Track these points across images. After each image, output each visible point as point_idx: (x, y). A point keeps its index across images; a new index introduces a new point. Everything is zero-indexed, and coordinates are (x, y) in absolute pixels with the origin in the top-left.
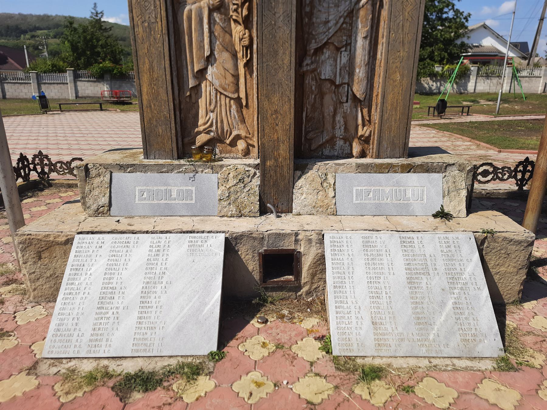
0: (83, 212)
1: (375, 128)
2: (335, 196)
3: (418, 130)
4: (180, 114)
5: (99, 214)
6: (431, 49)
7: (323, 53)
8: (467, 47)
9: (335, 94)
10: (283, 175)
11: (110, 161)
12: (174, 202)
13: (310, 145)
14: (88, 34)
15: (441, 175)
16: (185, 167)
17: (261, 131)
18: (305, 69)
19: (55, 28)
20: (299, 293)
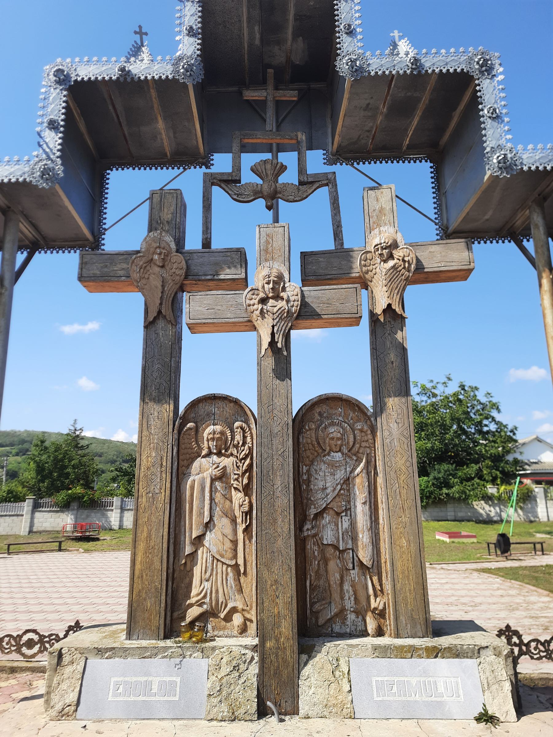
0: (42, 714)
1: (388, 599)
2: (350, 691)
3: (476, 577)
4: (173, 584)
5: (62, 716)
6: (478, 466)
7: (323, 517)
8: (523, 464)
9: (340, 560)
10: (286, 660)
11: (87, 644)
12: (153, 698)
13: (317, 618)
14: (60, 454)
16: (171, 651)
17: (260, 603)
18: (306, 534)
19: (19, 445)
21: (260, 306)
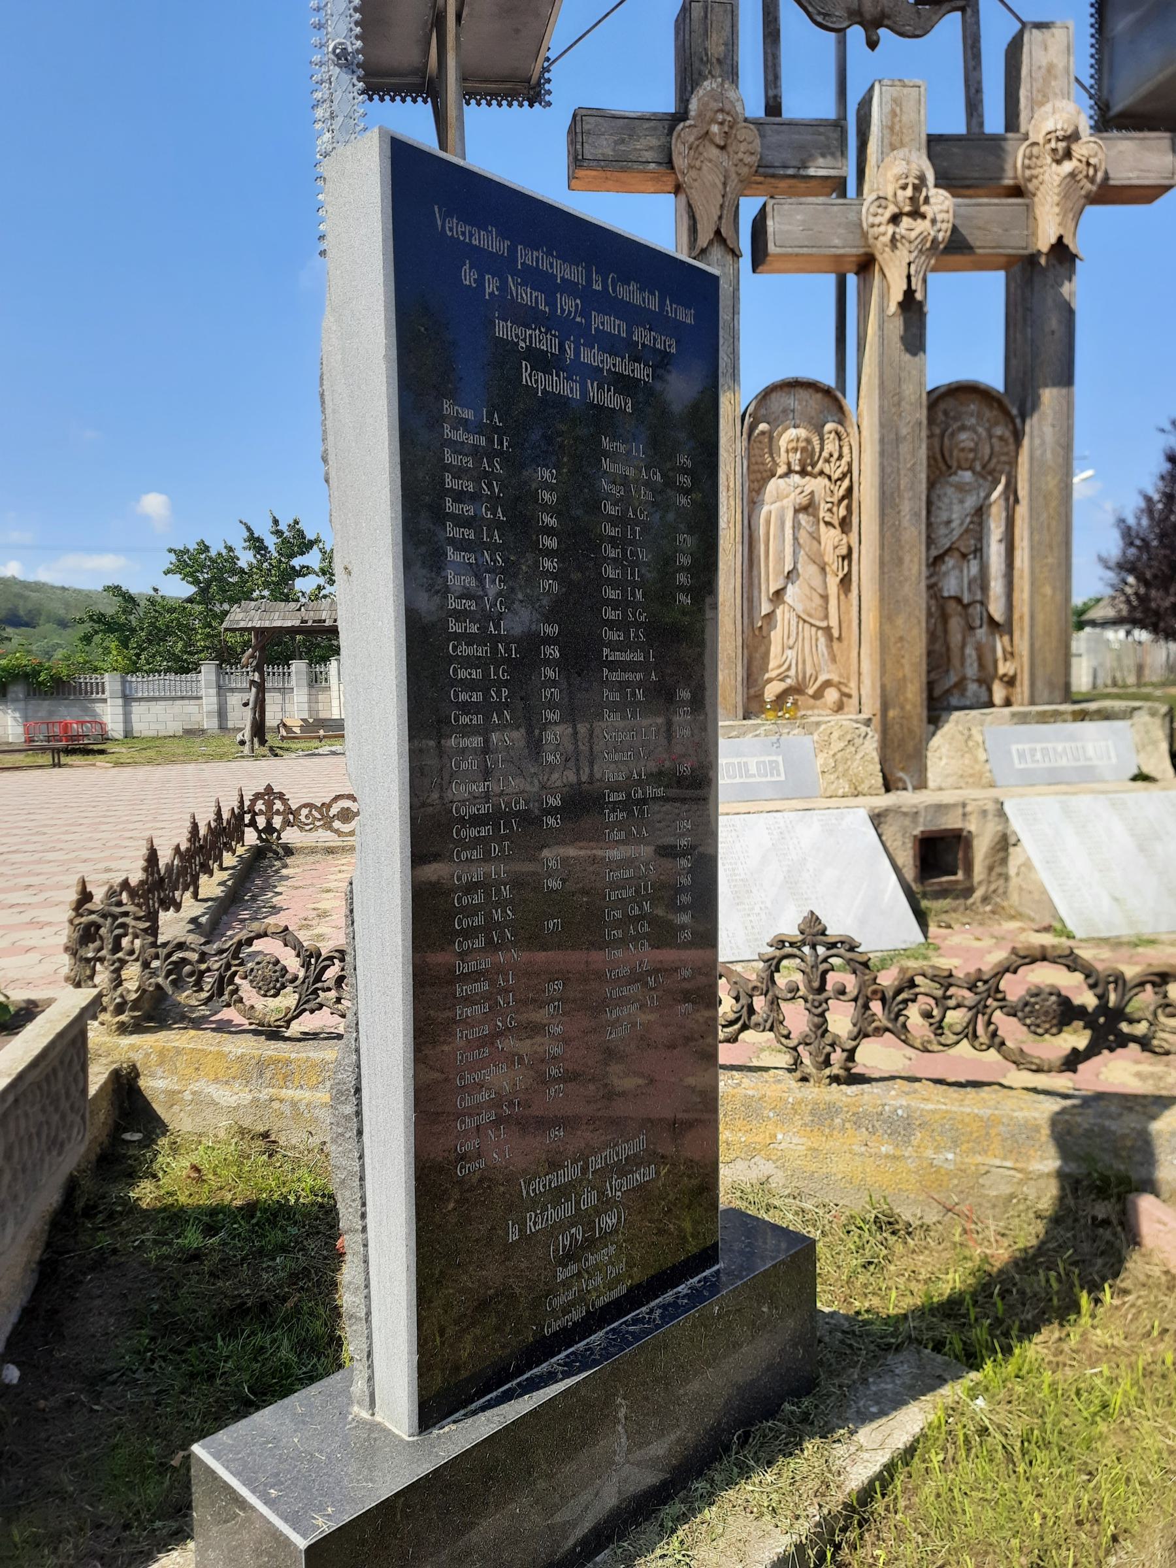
7: (944, 562)
15: (1128, 722)
20: (971, 901)
21: (891, 229)
